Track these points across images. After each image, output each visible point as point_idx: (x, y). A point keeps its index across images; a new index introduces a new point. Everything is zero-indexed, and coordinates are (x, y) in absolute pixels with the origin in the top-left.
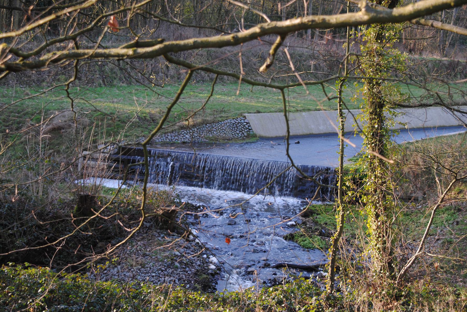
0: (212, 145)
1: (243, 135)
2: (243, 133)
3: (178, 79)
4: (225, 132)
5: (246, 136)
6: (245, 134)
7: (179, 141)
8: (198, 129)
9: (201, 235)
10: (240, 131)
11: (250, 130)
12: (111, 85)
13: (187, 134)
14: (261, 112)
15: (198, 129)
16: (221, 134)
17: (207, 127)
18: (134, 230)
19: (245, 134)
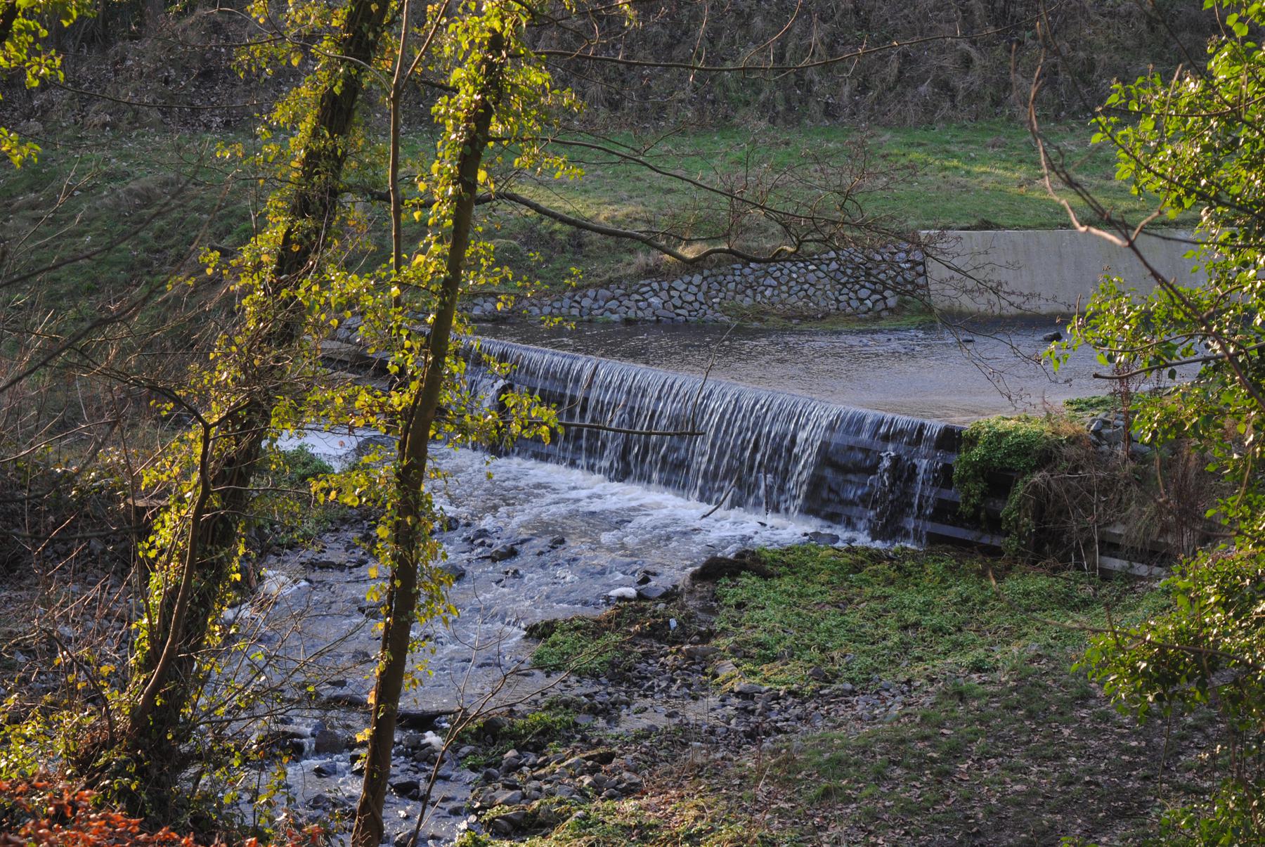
0: (742, 332)
1: (880, 305)
2: (885, 298)
3: (997, 103)
4: (811, 292)
5: (891, 310)
6: (892, 302)
7: (615, 317)
8: (705, 279)
9: (316, 787)
10: (874, 292)
11: (919, 286)
12: (724, 124)
13: (656, 295)
14: (998, 227)
15: (705, 279)
16: (793, 299)
17: (747, 271)
18: (800, 474)
19: (892, 302)
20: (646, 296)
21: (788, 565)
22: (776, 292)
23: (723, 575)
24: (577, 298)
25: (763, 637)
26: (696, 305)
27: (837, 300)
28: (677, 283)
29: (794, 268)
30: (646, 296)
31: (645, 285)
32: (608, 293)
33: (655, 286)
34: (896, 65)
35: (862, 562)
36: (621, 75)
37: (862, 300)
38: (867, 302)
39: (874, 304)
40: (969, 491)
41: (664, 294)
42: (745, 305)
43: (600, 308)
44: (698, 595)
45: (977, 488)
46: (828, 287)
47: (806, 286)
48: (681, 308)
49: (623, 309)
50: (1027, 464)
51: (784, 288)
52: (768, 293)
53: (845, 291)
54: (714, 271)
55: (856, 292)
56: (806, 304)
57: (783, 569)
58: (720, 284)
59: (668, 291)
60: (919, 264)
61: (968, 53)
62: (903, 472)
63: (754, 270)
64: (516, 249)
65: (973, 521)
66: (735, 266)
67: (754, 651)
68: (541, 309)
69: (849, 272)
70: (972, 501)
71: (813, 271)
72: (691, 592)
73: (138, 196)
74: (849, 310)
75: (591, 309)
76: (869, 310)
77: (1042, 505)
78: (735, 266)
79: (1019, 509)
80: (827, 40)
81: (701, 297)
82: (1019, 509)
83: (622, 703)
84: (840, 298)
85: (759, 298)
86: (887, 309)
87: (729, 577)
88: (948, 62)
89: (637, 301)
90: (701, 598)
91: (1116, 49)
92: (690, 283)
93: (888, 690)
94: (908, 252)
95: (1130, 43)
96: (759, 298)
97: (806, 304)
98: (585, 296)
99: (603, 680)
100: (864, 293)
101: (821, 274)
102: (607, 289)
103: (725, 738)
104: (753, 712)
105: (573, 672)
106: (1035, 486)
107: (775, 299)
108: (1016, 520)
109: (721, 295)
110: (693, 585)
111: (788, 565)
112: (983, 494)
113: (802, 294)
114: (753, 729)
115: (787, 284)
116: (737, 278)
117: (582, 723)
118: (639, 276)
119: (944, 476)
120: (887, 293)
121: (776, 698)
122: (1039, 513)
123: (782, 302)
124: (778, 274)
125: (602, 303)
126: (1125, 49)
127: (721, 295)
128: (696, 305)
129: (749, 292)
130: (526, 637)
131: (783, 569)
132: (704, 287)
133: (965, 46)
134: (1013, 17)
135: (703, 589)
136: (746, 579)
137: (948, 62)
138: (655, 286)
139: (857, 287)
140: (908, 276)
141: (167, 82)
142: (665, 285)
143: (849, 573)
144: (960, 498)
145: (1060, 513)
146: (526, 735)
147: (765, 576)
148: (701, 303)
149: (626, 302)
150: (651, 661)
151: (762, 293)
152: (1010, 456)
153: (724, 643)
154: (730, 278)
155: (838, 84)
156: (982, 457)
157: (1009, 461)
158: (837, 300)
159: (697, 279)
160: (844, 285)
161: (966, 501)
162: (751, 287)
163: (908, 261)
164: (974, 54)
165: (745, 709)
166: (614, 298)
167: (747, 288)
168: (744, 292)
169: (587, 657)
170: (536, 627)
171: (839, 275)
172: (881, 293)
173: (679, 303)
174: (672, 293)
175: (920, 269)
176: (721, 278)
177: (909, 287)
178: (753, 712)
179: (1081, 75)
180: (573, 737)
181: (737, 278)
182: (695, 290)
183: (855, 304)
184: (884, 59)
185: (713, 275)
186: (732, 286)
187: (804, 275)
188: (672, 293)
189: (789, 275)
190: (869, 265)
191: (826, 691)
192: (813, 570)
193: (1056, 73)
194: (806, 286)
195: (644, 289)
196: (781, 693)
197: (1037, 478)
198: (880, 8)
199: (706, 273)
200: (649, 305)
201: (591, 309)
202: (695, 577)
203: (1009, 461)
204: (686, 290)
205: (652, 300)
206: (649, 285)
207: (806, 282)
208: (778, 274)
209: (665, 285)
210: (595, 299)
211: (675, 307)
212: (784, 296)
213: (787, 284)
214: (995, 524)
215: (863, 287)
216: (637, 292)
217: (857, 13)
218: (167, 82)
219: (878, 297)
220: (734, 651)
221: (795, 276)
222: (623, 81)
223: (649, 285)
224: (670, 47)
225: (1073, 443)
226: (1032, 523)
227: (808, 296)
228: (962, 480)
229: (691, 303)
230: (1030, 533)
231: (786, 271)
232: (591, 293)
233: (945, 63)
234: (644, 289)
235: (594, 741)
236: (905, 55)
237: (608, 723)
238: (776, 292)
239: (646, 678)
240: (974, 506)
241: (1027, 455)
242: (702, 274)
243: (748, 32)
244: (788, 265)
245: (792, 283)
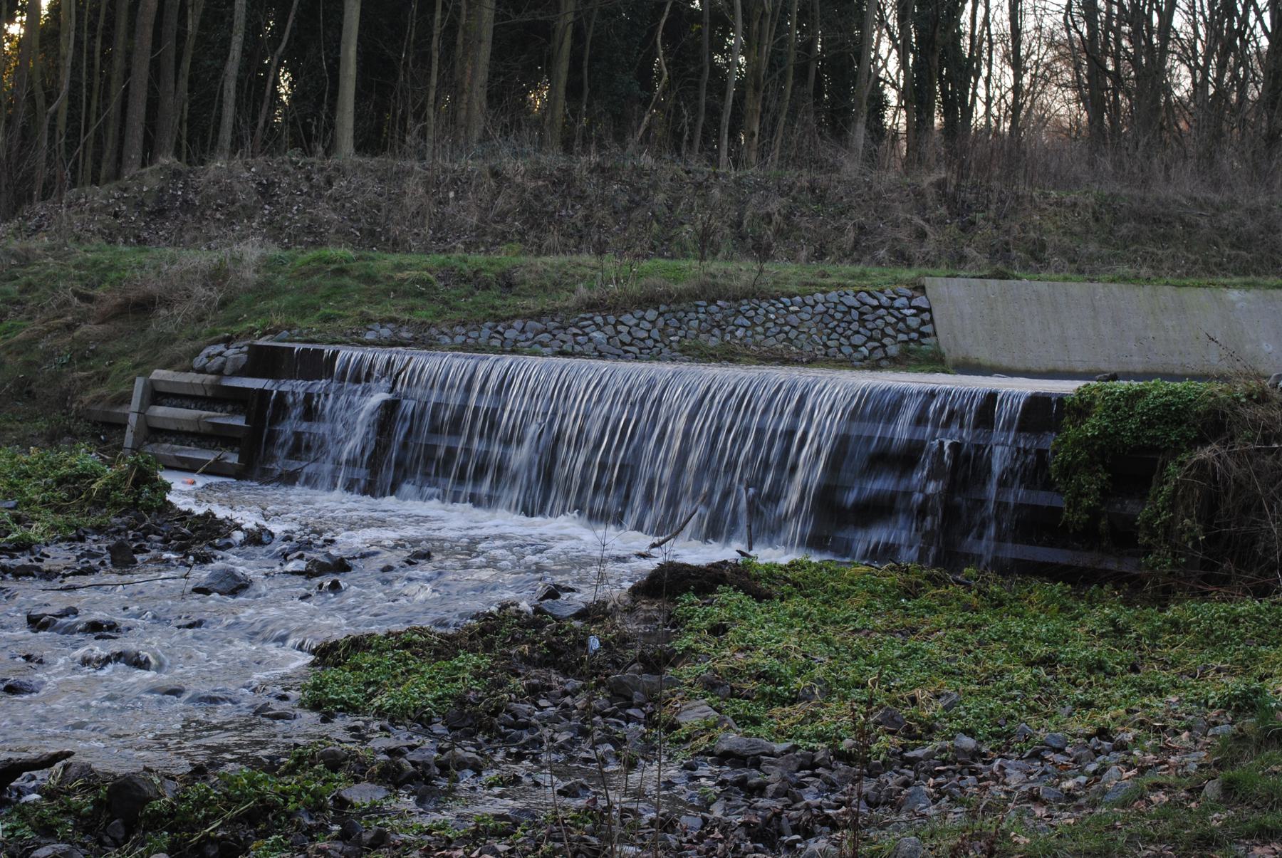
2: (884, 346)
4: (793, 334)
8: (661, 314)
10: (870, 339)
11: (923, 335)
13: (599, 327)
15: (661, 314)
16: (771, 341)
17: (713, 308)
20: (587, 330)
21: (795, 585)
22: (749, 333)
23: (686, 590)
24: (499, 328)
25: (768, 663)
26: (650, 343)
27: (825, 345)
28: (627, 318)
29: (772, 308)
30: (587, 330)
31: (586, 319)
32: (539, 326)
33: (599, 319)
34: (852, 235)
35: (918, 585)
36: (579, 231)
37: (855, 347)
38: (863, 349)
39: (871, 351)
40: (1080, 486)
41: (609, 329)
42: (711, 344)
43: (527, 340)
44: (641, 615)
45: (1092, 482)
46: (814, 330)
47: (787, 328)
48: (631, 345)
49: (557, 343)
50: (1182, 435)
51: (760, 329)
52: (739, 333)
53: (834, 336)
54: (673, 307)
55: (848, 338)
56: (787, 347)
57: (787, 588)
58: (679, 320)
59: (615, 326)
60: (924, 310)
61: (922, 228)
62: (966, 468)
63: (721, 308)
64: (429, 281)
65: (1088, 536)
66: (699, 303)
67: (750, 686)
68: (452, 339)
69: (838, 316)
70: (1086, 502)
71: (796, 312)
72: (630, 611)
73: (14, 255)
74: (840, 356)
75: (516, 341)
76: (865, 358)
77: (1211, 493)
78: (699, 303)
79: (1173, 508)
80: (783, 212)
81: (655, 334)
82: (1173, 508)
83: (462, 765)
84: (829, 343)
85: (728, 337)
86: (886, 357)
87: (697, 593)
88: (903, 234)
89: (575, 335)
90: (647, 620)
91: (1065, 234)
92: (643, 318)
93: (1059, 750)
94: (910, 299)
95: (1077, 229)
96: (728, 337)
97: (787, 347)
98: (510, 327)
99: (439, 728)
100: (857, 340)
101: (805, 317)
102: (539, 321)
103: (700, 838)
104: (760, 789)
105: (380, 713)
106: (1202, 465)
107: (750, 340)
108: (1168, 526)
109: (681, 333)
110: (634, 601)
111: (795, 585)
112: (1103, 491)
113: (782, 336)
114: (767, 822)
115: (763, 324)
116: (702, 316)
117: (357, 800)
118: (579, 310)
119: (1034, 471)
120: (886, 341)
121: (810, 764)
122: (1210, 509)
123: (756, 344)
124: (752, 313)
125: (530, 335)
126: (1072, 234)
127: (681, 333)
128: (650, 343)
129: (716, 331)
130: (313, 664)
131: (787, 588)
132: (661, 322)
133: (917, 220)
134: (964, 202)
135: (648, 607)
136: (724, 595)
137: (903, 234)
138: (599, 319)
139: (849, 333)
140: (914, 322)
141: (116, 215)
142: (611, 319)
143: (898, 597)
144: (1060, 501)
145: (1246, 509)
146: (206, 822)
147: (759, 597)
148: (656, 341)
149: (561, 335)
150: (543, 703)
151: (732, 332)
152: (1150, 425)
153: (686, 671)
154: (692, 315)
155: (795, 250)
156: (1103, 432)
157: (1150, 433)
158: (825, 345)
159: (651, 314)
160: (834, 330)
161: (1074, 504)
162: (719, 326)
163: (911, 307)
164: (927, 228)
165: (742, 783)
166: (545, 331)
167: (713, 327)
168: (709, 331)
169: (418, 688)
170: (335, 646)
171: (827, 319)
172: (879, 341)
173: (627, 339)
174: (620, 328)
175: (926, 316)
176: (681, 314)
177: (914, 335)
178: (760, 789)
179: (1032, 253)
180: (324, 829)
181: (702, 316)
182: (649, 326)
183: (847, 350)
184: (840, 230)
185: (670, 311)
186: (694, 324)
187: (784, 316)
188: (620, 328)
189: (765, 316)
190: (863, 309)
191: (919, 753)
192: (838, 592)
193: (1008, 251)
194: (787, 328)
195: (585, 323)
196: (820, 756)
197: (1204, 453)
198: (836, 187)
199: (663, 308)
200: (590, 340)
201: (516, 341)
202: (636, 591)
203: (1150, 433)
204: (637, 325)
205: (595, 334)
206: (591, 319)
207: (787, 324)
208: (752, 313)
209: (611, 319)
210: (523, 331)
211: (623, 343)
212: (759, 338)
213: (763, 324)
214: (1124, 538)
215: (858, 332)
216: (575, 325)
217: (813, 191)
218: (116, 215)
219: (877, 344)
220: (711, 686)
221: (772, 316)
222: (581, 237)
223: (591, 319)
224: (628, 210)
225: (1257, 401)
226: (1198, 528)
227: (788, 339)
228: (1067, 471)
229: (643, 340)
230: (1196, 544)
231: (761, 311)
232: (518, 324)
233: (899, 236)
234: (585, 323)
235: (367, 837)
236: (861, 228)
237: (420, 802)
238: (749, 333)
239: (527, 726)
240: (1089, 510)
241: (1180, 423)
242: (657, 309)
243: (706, 201)
244: (764, 304)
245: (771, 324)
